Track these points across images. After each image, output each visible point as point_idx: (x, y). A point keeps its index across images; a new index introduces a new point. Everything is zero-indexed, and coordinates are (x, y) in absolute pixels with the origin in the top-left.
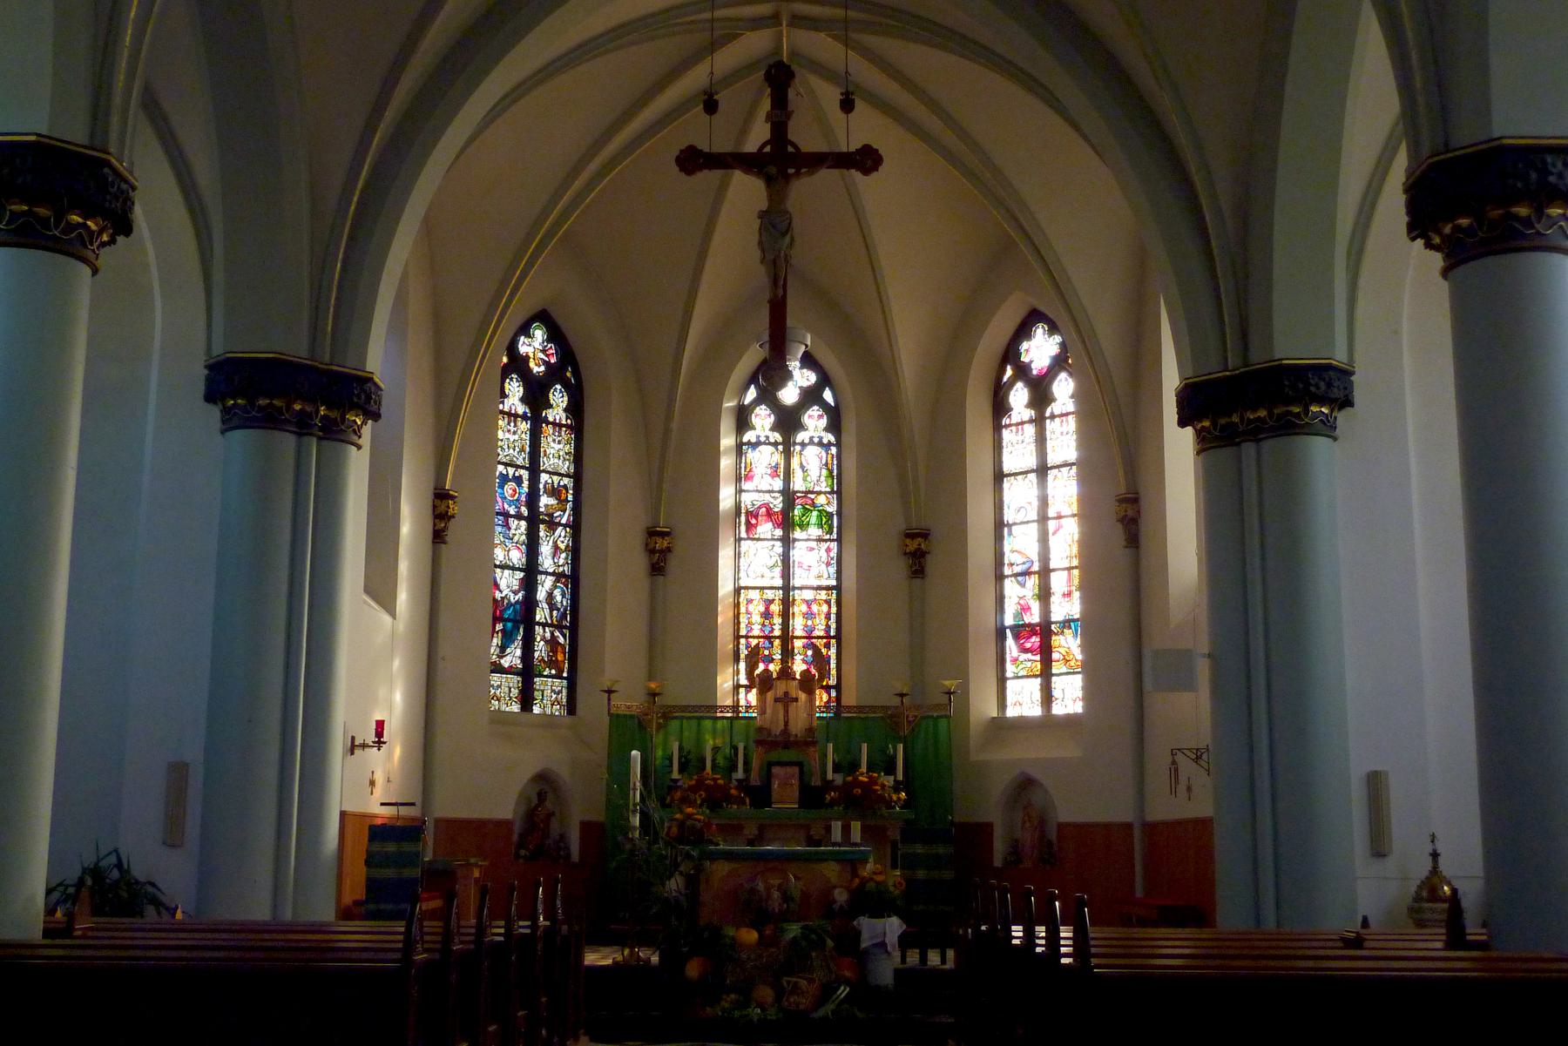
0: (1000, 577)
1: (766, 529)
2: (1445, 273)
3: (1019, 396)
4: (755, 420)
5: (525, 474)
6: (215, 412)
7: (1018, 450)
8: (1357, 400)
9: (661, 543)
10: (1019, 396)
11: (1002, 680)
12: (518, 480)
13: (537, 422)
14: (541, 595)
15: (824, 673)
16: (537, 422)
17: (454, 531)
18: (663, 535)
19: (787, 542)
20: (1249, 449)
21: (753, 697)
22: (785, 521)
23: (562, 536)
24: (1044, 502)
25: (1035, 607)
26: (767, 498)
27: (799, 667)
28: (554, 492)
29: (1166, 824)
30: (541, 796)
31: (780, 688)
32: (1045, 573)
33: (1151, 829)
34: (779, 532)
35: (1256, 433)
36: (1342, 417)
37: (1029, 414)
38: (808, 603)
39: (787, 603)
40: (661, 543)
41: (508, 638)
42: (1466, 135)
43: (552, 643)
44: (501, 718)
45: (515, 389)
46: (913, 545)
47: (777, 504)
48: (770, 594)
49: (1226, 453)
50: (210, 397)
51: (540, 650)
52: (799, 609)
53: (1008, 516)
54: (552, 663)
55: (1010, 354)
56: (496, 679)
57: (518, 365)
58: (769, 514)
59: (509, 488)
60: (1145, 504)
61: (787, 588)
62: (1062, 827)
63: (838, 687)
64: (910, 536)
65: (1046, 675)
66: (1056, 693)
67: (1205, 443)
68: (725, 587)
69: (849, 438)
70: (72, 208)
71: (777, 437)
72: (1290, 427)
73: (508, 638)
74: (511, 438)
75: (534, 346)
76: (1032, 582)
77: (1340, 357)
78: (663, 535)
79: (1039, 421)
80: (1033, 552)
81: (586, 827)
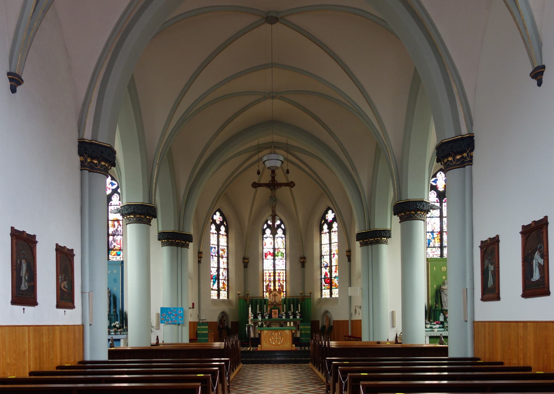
0: (321, 267)
1: (270, 257)
2: (400, 222)
3: (325, 227)
4: (266, 232)
5: (216, 247)
6: (160, 242)
7: (325, 238)
8: (392, 236)
9: (246, 261)
10: (325, 227)
11: (321, 290)
12: (215, 248)
13: (218, 234)
14: (221, 273)
15: (283, 289)
16: (218, 234)
17: (203, 260)
18: (247, 259)
19: (274, 259)
20: (370, 246)
21: (267, 294)
22: (274, 255)
23: (225, 260)
24: (331, 251)
25: (329, 274)
26: (269, 250)
27: (277, 288)
28: (223, 250)
29: (355, 320)
30: (223, 317)
31: (274, 293)
32: (331, 267)
33: (353, 322)
34: (272, 258)
35: (372, 243)
36: (389, 240)
37: (327, 231)
38: (279, 273)
39: (274, 273)
40: (246, 261)
41: (214, 282)
42: (404, 199)
43: (223, 283)
44: (213, 300)
45: (213, 227)
46: (302, 260)
47: (272, 251)
48: (270, 271)
49: (365, 247)
50: (159, 240)
51: (221, 285)
52: (277, 274)
53: (323, 254)
54: (224, 288)
55: (324, 217)
56: (212, 291)
57: (214, 222)
58: (270, 253)
59: (213, 249)
60: (352, 253)
61: (274, 270)
62: (334, 321)
63: (286, 292)
64: (301, 258)
65: (331, 289)
66: (333, 293)
67: (362, 245)
68: (261, 269)
69: (288, 236)
70: (147, 215)
71: (271, 236)
72: (378, 242)
73: (214, 282)
74: (213, 240)
75: (217, 217)
76: (328, 268)
77: (389, 228)
78: (247, 259)
79: (330, 233)
80: (328, 261)
81: (232, 322)
